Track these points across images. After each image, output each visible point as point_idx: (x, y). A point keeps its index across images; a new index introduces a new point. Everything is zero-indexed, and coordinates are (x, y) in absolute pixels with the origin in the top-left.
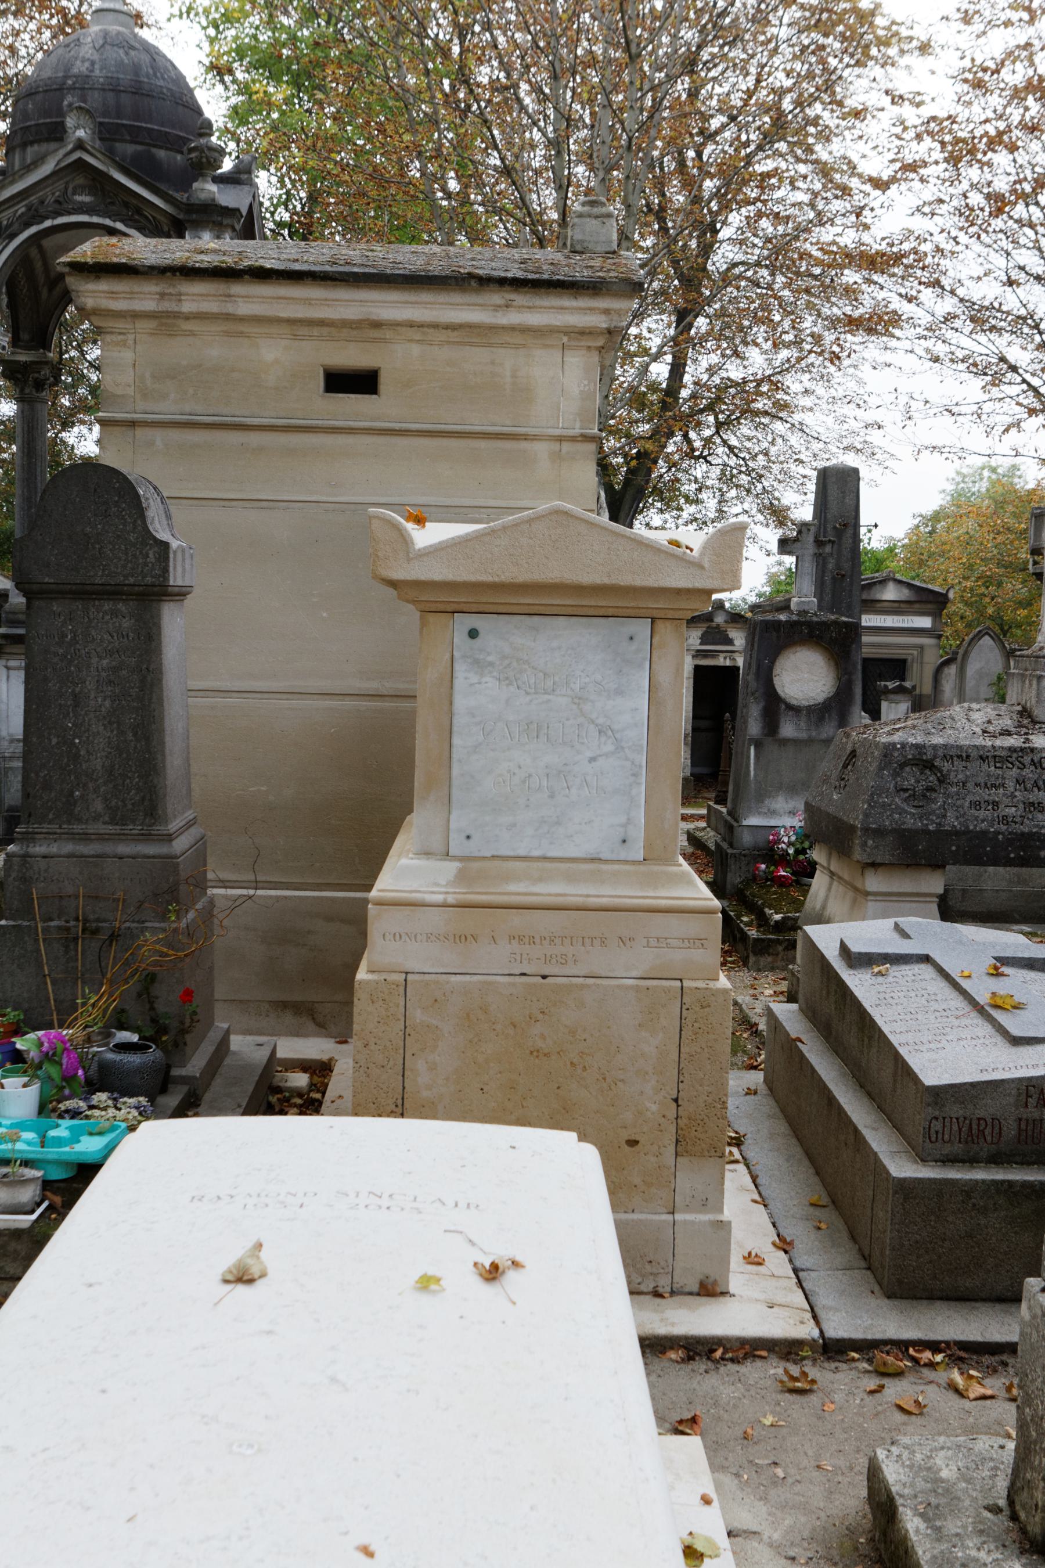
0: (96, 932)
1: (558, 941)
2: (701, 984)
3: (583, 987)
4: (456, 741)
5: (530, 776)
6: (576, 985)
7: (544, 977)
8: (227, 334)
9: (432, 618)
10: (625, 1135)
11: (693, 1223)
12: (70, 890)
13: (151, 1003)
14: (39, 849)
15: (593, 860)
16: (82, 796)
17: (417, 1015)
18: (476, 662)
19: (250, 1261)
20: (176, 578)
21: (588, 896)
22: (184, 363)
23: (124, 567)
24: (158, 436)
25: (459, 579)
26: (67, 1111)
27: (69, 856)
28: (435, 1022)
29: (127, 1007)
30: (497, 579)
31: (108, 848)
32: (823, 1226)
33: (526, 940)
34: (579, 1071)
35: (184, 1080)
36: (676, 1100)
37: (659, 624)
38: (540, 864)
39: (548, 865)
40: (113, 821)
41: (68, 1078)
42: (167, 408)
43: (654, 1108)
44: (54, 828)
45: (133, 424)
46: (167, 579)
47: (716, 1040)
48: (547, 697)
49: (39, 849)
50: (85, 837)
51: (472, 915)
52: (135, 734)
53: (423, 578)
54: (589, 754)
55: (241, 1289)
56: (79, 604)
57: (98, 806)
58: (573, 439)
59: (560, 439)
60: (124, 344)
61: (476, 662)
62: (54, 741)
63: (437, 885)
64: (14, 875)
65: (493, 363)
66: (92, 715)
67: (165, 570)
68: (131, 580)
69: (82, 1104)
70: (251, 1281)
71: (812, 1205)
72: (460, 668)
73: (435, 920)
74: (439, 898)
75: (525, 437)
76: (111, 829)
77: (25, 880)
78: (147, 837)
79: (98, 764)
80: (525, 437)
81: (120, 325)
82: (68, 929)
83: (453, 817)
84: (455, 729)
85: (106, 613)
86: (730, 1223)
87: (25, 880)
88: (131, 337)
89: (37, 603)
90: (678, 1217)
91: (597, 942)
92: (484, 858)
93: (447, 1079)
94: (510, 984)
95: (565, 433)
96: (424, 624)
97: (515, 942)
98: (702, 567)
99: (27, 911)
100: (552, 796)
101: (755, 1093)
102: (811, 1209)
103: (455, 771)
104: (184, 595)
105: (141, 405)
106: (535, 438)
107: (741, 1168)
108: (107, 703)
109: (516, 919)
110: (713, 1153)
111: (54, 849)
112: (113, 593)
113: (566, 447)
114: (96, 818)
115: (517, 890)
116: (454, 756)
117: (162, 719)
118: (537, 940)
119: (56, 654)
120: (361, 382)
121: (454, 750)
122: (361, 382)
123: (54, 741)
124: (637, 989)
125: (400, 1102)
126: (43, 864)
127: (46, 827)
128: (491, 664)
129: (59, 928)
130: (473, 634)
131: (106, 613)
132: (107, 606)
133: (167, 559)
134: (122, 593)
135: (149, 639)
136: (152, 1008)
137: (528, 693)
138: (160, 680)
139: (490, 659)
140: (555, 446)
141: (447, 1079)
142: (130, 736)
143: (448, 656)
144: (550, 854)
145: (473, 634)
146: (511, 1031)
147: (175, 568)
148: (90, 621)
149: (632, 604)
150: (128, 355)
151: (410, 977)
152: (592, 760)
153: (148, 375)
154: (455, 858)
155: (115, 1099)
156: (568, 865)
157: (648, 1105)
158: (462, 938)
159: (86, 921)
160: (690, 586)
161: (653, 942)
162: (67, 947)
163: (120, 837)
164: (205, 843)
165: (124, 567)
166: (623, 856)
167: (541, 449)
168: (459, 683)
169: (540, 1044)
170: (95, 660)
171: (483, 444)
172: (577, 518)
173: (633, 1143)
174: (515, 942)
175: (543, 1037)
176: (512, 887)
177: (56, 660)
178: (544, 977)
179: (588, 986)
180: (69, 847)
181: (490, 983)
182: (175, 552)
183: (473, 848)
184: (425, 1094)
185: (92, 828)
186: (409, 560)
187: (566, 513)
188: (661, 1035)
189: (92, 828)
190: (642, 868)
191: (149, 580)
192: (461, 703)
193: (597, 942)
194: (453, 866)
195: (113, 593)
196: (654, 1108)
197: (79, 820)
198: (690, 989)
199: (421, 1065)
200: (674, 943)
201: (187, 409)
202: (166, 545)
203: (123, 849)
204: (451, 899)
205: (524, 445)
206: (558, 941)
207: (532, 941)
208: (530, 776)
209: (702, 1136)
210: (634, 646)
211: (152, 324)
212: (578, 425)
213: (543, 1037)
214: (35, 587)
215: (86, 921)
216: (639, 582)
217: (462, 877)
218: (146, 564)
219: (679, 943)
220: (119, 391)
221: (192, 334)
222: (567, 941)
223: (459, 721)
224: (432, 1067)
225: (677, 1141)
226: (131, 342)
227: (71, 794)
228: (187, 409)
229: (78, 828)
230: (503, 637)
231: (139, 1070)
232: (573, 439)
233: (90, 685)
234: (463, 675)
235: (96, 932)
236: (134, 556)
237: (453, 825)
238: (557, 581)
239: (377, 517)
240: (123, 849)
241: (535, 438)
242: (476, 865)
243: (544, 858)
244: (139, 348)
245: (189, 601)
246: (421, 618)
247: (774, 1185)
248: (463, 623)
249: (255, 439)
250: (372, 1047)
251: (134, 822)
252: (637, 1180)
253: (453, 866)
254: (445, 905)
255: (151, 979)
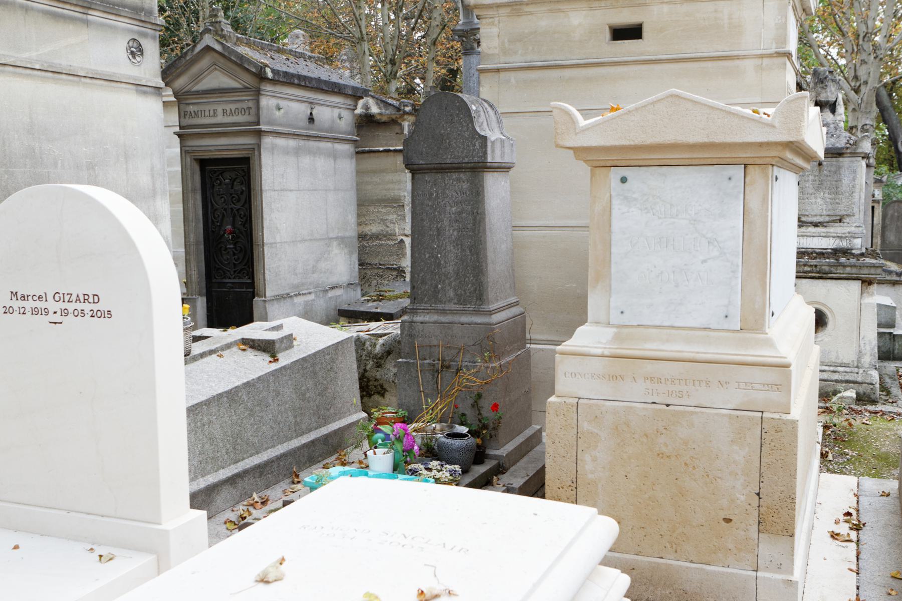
0: (448, 367)
1: (677, 382)
2: (776, 416)
3: (692, 413)
4: (614, 250)
5: (662, 272)
6: (688, 412)
7: (668, 405)
8: (551, 11)
9: (598, 170)
10: (723, 514)
11: (769, 579)
12: (435, 342)
13: (479, 410)
14: (419, 318)
15: (705, 329)
16: (442, 288)
17: (585, 426)
18: (626, 198)
19: (271, 570)
20: (494, 156)
21: (698, 353)
22: (526, 31)
23: (462, 152)
24: (512, 76)
25: (608, 144)
26: (411, 470)
27: (435, 322)
28: (596, 431)
29: (466, 412)
30: (632, 143)
31: (456, 318)
32: (893, 593)
33: (655, 380)
34: (691, 469)
35: (496, 457)
36: (758, 494)
37: (750, 168)
38: (668, 331)
39: (673, 331)
40: (459, 303)
41: (408, 451)
42: (517, 60)
43: (743, 498)
44: (428, 306)
45: (498, 70)
46: (486, 158)
47: (786, 455)
48: (673, 220)
49: (419, 318)
50: (443, 312)
51: (621, 361)
52: (471, 251)
53: (585, 145)
54: (702, 258)
55: (261, 585)
56: (439, 176)
57: (451, 293)
58: (770, 56)
59: (762, 56)
60: (493, 24)
61: (626, 198)
62: (427, 256)
63: (600, 342)
64: (406, 333)
65: (716, 11)
66: (447, 240)
67: (485, 153)
68: (466, 160)
69: (422, 466)
70: (268, 582)
71: (892, 577)
72: (616, 203)
73: (597, 365)
74: (599, 351)
75: (738, 57)
76: (458, 307)
77: (411, 336)
78: (477, 312)
79: (450, 269)
80: (738, 57)
81: (491, 12)
82: (434, 365)
83: (612, 299)
84: (613, 242)
85: (454, 180)
86: (797, 582)
87: (411, 336)
88: (497, 19)
89: (417, 176)
90: (759, 574)
91: (703, 384)
92: (632, 326)
93: (604, 468)
94: (644, 408)
95: (765, 52)
96: (593, 175)
97: (648, 382)
98: (774, 127)
99: (412, 354)
100: (677, 286)
101: (888, 495)
102: (891, 580)
103: (614, 269)
104: (509, 168)
105: (502, 59)
106: (744, 57)
107: (853, 546)
108: (455, 233)
109: (649, 366)
110: (785, 533)
111: (427, 318)
112: (457, 168)
113: (766, 61)
114: (450, 301)
115: (651, 347)
116: (613, 259)
117: (486, 242)
118: (663, 381)
119: (427, 205)
120: (632, 32)
121: (613, 256)
122: (632, 32)
123: (427, 256)
124: (730, 416)
125: (574, 480)
126: (420, 327)
127: (423, 306)
128: (635, 199)
129: (429, 364)
130: (624, 180)
131: (454, 180)
132: (455, 176)
133: (486, 146)
134: (460, 168)
135: (477, 194)
136: (480, 414)
137: (659, 218)
138: (484, 219)
139: (635, 196)
140: (758, 61)
141: (604, 468)
142: (468, 252)
143: (608, 195)
144: (676, 324)
145: (624, 180)
146: (645, 440)
147: (493, 151)
148: (446, 185)
149: (728, 155)
150: (495, 30)
151: (581, 401)
152: (704, 261)
153: (506, 40)
154: (613, 326)
155: (442, 465)
156: (687, 332)
157: (738, 496)
158: (614, 377)
159: (443, 361)
160: (766, 140)
161: (742, 386)
162: (433, 375)
163: (463, 312)
164: (525, 317)
165: (462, 152)
166: (726, 327)
167: (749, 64)
168: (615, 212)
169: (664, 449)
170: (448, 208)
171: (709, 64)
172: (685, 99)
173: (728, 521)
174: (648, 382)
175: (666, 445)
176: (648, 346)
177: (427, 208)
178: (668, 405)
179: (696, 413)
180: (435, 318)
181: (631, 407)
182: (493, 143)
183: (625, 320)
184: (590, 476)
185: (447, 307)
186: (576, 134)
187: (677, 96)
188: (747, 449)
189: (447, 307)
190: (739, 335)
191: (476, 159)
192: (616, 225)
193: (703, 384)
194: (612, 331)
195: (457, 168)
196: (743, 498)
197: (441, 302)
198: (767, 418)
199: (588, 458)
200: (757, 386)
201: (529, 58)
202: (484, 139)
203: (464, 319)
204: (607, 352)
205: (737, 62)
206: (677, 382)
207: (659, 381)
208: (662, 272)
209: (777, 520)
210: (732, 184)
211: (508, 10)
212: (774, 46)
213: (666, 445)
214: (415, 167)
215: (443, 361)
216: (729, 139)
217: (617, 338)
218: (474, 150)
219: (761, 387)
220: (490, 52)
221: (531, 13)
222: (683, 382)
223: (615, 237)
224: (595, 459)
225: (759, 522)
226: (496, 22)
227: (436, 287)
228: (529, 59)
229: (440, 306)
230: (643, 181)
231: (457, 449)
232: (770, 56)
233: (446, 223)
234: (618, 208)
235: (448, 367)
236: (468, 146)
237: (612, 304)
238: (673, 142)
239: (556, 108)
240: (464, 319)
241: (744, 57)
242: (625, 331)
243: (673, 327)
244: (501, 25)
245: (512, 171)
246: (592, 171)
247: (871, 560)
248: (615, 175)
249: (567, 73)
250: (558, 444)
251: (470, 303)
252: (731, 546)
253: (612, 331)
254: (603, 356)
255: (479, 396)
